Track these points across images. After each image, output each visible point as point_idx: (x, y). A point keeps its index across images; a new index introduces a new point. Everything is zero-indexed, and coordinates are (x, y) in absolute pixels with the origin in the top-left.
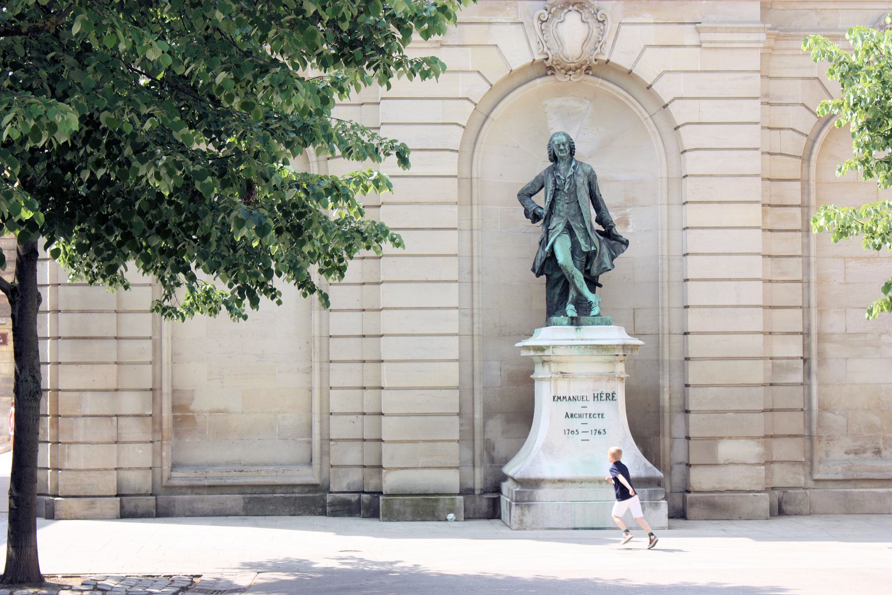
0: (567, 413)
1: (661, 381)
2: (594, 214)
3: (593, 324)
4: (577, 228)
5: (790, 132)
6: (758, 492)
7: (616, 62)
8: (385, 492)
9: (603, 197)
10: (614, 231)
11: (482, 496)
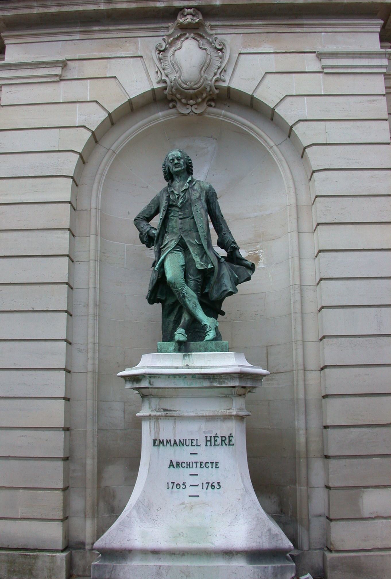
1: (296, 423)
3: (206, 350)
4: (191, 244)
10: (237, 254)
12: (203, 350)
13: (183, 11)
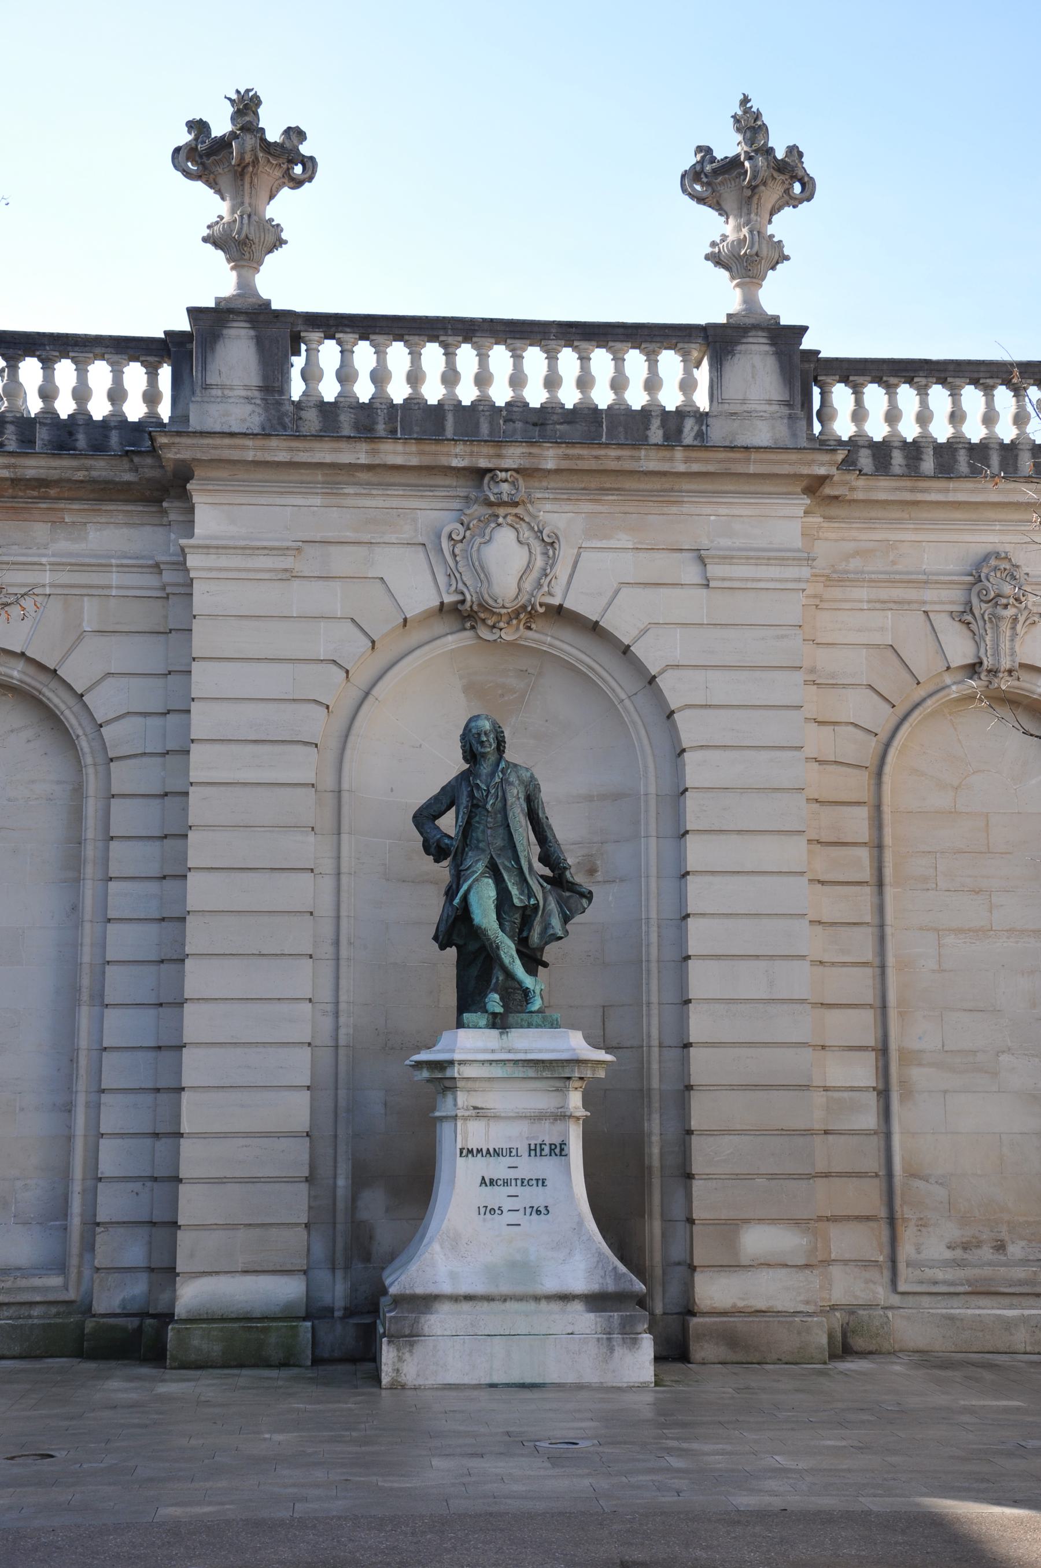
0: (483, 1178)
1: (646, 1125)
2: (536, 850)
3: (529, 1026)
4: (506, 868)
5: (851, 728)
6: (809, 1314)
7: (574, 609)
8: (178, 1316)
9: (551, 821)
11: (347, 1320)
12: (526, 1026)
13: (493, 473)
